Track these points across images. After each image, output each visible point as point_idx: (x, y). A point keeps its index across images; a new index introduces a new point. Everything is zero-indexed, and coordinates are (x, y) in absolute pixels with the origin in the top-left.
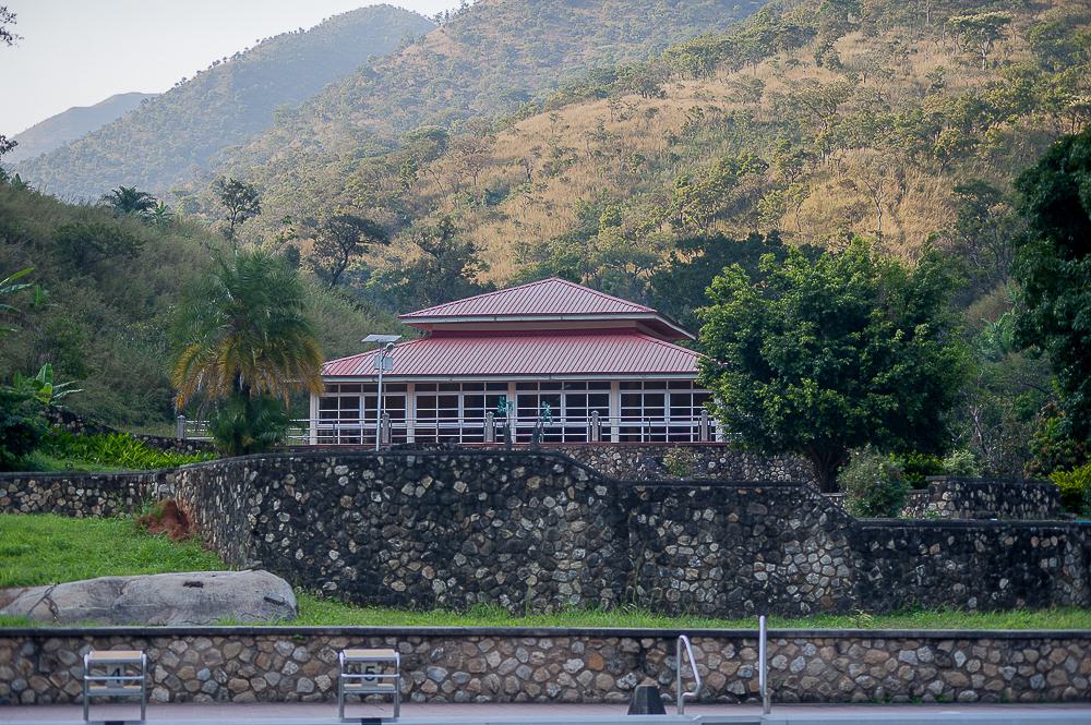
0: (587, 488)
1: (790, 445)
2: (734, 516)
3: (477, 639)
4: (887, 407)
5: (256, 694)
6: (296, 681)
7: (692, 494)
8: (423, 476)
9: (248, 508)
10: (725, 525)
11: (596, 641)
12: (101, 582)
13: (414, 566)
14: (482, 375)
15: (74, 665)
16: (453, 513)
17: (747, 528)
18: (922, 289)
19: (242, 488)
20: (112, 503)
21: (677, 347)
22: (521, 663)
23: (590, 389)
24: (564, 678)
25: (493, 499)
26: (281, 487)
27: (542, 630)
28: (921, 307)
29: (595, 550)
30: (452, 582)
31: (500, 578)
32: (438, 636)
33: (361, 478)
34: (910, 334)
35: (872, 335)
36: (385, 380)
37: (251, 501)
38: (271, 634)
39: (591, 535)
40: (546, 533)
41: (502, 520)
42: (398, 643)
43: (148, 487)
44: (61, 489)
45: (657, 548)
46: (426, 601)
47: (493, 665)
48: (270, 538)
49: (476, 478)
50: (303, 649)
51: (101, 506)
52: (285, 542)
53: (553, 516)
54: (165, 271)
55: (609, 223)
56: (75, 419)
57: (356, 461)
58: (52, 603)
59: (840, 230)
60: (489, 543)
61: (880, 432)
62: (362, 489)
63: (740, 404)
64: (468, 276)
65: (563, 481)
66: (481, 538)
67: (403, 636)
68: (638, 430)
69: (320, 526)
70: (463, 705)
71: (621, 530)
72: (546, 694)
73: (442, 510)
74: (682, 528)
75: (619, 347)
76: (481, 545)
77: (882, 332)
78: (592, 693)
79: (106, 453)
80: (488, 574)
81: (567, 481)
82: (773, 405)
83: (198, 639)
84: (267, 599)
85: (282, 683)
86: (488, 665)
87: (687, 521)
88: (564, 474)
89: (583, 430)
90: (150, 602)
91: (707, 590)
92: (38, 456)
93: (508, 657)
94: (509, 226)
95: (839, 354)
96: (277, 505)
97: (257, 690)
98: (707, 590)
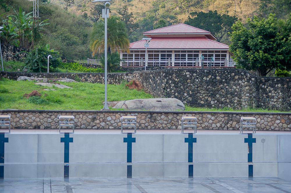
0: (250, 79)
1: (254, 67)
2: (286, 86)
3: (255, 115)
4: (281, 58)
5: (202, 127)
6: (212, 125)
7: (275, 80)
8: (209, 75)
9: (162, 83)
10: (283, 88)
11: (284, 116)
12: (136, 100)
13: (206, 98)
14: (166, 49)
15: (160, 120)
16: (216, 84)
17: (289, 89)
18: (289, 28)
19: (160, 78)
20: (112, 81)
21: (223, 44)
22: (265, 121)
23: (208, 52)
24: (275, 125)
25: (226, 81)
26: (172, 77)
27: (271, 113)
28: (288, 32)
29: (251, 94)
30: (216, 101)
31: (228, 101)
32: (246, 114)
33: (193, 75)
34: (287, 40)
35: (277, 40)
36: (148, 49)
37: (163, 81)
38: (206, 113)
39: (250, 90)
40: (239, 90)
41: (228, 86)
42: (236, 116)
43: (123, 77)
44: (98, 77)
45: (266, 94)
46: (210, 106)
47: (259, 121)
48: (168, 90)
49: (222, 76)
50: (213, 117)
51: (109, 81)
52: (173, 91)
53: (241, 86)
54: (58, 19)
55: (162, 7)
56: (65, 59)
57: (191, 71)
58: (126, 105)
59: (225, 10)
60: (225, 92)
61: (279, 65)
62: (193, 78)
63: (242, 57)
64: (131, 21)
65: (244, 77)
66: (223, 91)
67: (195, 113)
68: (192, 63)
69: (182, 87)
70: (277, 131)
71: (258, 89)
72: (271, 129)
73: (213, 84)
74: (273, 89)
75: (202, 42)
76: (223, 92)
77: (280, 39)
78: (282, 129)
79: (73, 68)
80: (225, 100)
81: (245, 77)
82: (251, 58)
83: (189, 114)
84: (178, 105)
85: (209, 125)
86: (257, 121)
87: (274, 87)
88: (244, 75)
89: (139, 63)
90: (149, 105)
91: (278, 104)
92: (58, 69)
93: (262, 119)
94: (134, 8)
95: (269, 44)
96: (170, 82)
97: (203, 127)
98: (278, 104)
